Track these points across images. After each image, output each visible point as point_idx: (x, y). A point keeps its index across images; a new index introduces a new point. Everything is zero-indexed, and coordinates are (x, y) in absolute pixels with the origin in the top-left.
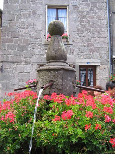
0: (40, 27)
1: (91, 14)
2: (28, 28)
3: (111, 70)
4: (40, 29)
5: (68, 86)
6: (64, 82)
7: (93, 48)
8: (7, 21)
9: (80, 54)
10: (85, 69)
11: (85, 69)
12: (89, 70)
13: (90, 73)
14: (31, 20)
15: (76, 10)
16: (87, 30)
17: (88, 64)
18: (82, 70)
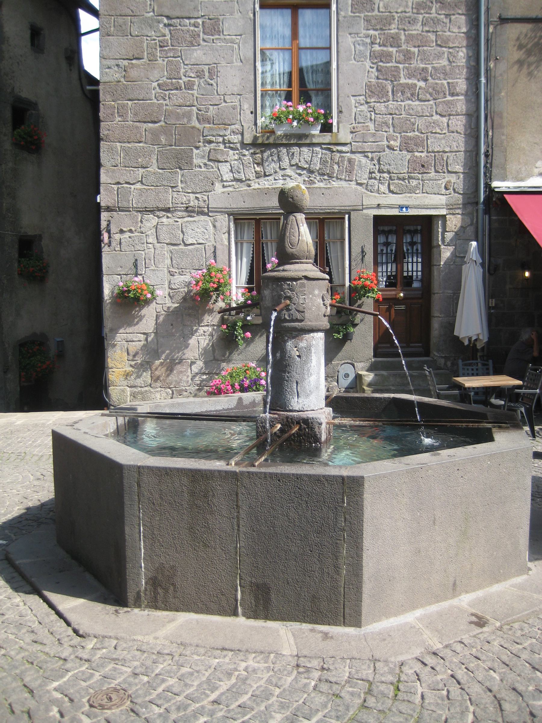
0: (237, 81)
1: (417, 29)
2: (189, 86)
3: (483, 231)
4: (236, 90)
5: (315, 306)
6: (308, 298)
7: (423, 155)
8: (116, 62)
9: (378, 175)
10: (394, 228)
11: (394, 228)
12: (409, 232)
13: (412, 244)
14: (204, 58)
15: (362, 15)
16: (404, 88)
17: (404, 212)
18: (383, 232)
